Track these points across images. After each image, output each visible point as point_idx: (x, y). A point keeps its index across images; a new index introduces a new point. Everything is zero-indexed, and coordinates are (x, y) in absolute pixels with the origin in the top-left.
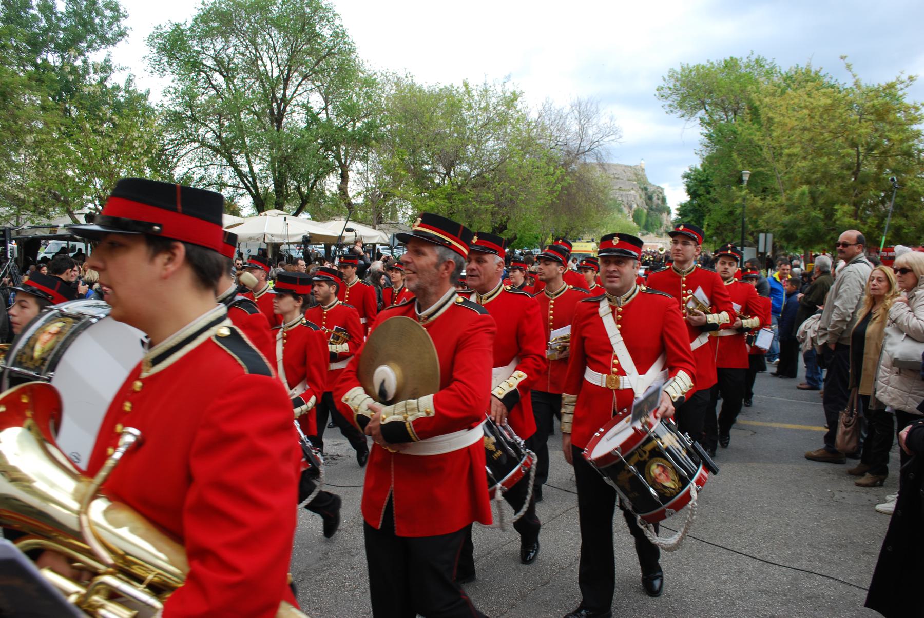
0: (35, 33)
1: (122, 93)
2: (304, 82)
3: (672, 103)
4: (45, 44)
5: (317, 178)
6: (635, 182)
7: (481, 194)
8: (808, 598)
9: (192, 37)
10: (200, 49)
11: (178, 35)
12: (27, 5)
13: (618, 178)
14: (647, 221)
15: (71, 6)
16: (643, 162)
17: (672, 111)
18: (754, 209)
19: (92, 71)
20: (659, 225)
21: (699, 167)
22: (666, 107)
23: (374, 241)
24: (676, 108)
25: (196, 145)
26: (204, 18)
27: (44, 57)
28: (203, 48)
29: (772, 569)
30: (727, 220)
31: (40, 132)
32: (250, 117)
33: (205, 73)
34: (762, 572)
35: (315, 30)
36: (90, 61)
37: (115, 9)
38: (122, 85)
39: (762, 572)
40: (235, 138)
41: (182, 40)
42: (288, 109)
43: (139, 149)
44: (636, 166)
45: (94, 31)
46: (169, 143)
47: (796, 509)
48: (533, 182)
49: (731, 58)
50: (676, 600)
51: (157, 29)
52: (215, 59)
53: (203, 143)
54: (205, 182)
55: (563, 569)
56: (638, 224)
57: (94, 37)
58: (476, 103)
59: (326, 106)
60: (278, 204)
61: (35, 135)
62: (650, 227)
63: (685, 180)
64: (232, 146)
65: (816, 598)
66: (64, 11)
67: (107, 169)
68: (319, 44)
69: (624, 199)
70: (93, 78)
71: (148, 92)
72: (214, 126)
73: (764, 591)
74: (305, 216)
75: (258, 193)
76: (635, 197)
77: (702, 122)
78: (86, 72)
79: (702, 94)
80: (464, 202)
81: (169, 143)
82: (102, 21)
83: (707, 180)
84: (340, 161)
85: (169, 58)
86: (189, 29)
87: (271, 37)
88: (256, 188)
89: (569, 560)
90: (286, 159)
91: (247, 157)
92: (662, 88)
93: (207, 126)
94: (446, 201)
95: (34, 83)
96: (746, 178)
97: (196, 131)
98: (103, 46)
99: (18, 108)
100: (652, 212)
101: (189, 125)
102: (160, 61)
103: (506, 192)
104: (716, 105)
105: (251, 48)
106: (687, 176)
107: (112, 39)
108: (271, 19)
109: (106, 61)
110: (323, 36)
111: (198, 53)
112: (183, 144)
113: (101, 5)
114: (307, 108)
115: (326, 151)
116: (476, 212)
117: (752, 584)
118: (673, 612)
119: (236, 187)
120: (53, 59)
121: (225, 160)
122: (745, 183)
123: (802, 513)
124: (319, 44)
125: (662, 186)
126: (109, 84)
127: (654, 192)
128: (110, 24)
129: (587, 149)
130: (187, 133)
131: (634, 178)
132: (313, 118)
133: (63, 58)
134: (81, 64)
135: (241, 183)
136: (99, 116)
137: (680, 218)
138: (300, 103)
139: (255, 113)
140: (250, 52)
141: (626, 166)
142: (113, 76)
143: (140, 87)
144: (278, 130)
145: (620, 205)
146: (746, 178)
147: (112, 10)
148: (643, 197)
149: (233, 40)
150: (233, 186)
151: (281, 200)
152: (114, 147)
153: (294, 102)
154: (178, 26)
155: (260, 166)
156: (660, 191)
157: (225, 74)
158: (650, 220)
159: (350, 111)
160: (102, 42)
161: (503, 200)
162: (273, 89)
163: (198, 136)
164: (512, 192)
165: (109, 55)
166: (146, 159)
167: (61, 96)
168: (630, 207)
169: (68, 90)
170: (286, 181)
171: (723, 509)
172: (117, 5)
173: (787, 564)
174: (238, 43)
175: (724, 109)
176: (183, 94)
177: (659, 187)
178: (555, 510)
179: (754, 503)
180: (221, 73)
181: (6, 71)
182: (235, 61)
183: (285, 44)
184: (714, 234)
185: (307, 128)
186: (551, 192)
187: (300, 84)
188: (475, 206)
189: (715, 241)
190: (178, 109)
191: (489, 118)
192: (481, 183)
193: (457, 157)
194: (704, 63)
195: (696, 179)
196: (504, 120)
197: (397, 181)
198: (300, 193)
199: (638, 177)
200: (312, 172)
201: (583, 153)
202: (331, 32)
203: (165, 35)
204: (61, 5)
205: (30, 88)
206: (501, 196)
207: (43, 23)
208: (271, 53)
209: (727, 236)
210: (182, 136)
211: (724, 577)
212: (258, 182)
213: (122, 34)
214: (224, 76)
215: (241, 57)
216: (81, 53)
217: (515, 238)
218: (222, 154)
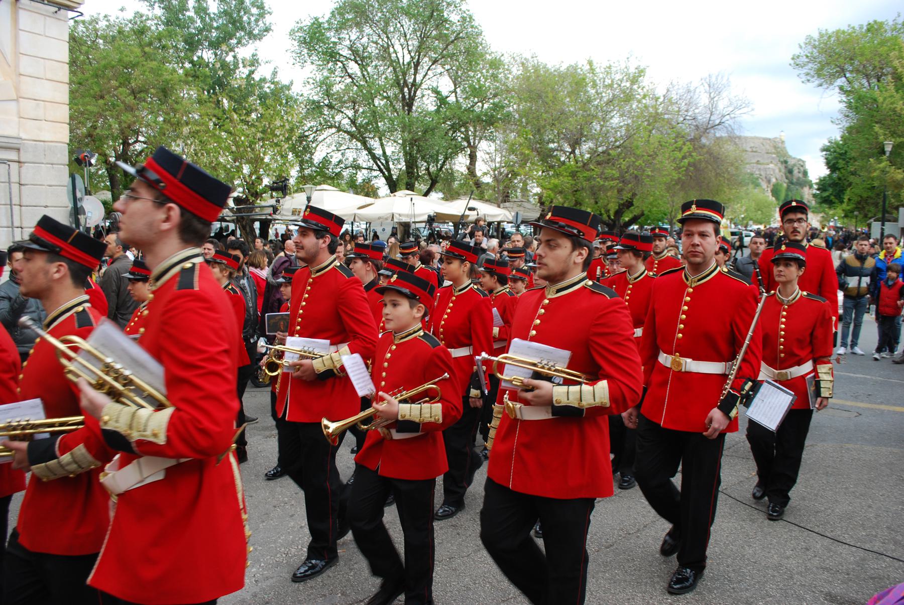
0: (190, 34)
1: (267, 85)
2: (433, 67)
3: (809, 71)
4: (199, 42)
5: (446, 159)
6: (774, 156)
7: (606, 171)
8: (871, 578)
9: (329, 29)
10: (337, 40)
11: (317, 28)
12: (183, 8)
15: (222, 6)
16: (782, 134)
17: (808, 81)
18: (894, 181)
19: (241, 65)
22: (802, 76)
23: (499, 219)
24: (813, 77)
25: (334, 130)
26: (340, 11)
27: (200, 54)
28: (339, 39)
29: (841, 549)
30: (870, 194)
31: (196, 123)
32: (382, 103)
33: (342, 62)
34: (830, 550)
35: (443, 16)
36: (240, 56)
37: (261, 7)
38: (269, 77)
39: (830, 550)
40: (367, 124)
41: (320, 32)
42: (419, 93)
43: (281, 137)
44: (776, 138)
45: (243, 29)
46: (309, 130)
47: (884, 492)
48: (659, 158)
49: (875, 22)
50: (734, 570)
51: (298, 23)
52: (350, 49)
53: (339, 129)
54: (342, 165)
55: (629, 534)
56: (777, 199)
57: (243, 34)
58: (600, 80)
59: (456, 88)
60: (409, 185)
61: (190, 126)
63: (824, 153)
64: (366, 129)
65: (880, 579)
66: (216, 12)
67: (253, 156)
68: (447, 29)
69: (762, 173)
70: (242, 72)
71: (292, 83)
72: (350, 113)
73: (826, 568)
74: (435, 196)
75: (391, 175)
76: (774, 170)
78: (236, 66)
79: (841, 60)
80: (588, 179)
81: (309, 130)
82: (249, 19)
83: (846, 152)
84: (469, 142)
85: (309, 49)
86: (327, 21)
87: (402, 26)
88: (389, 170)
89: (637, 527)
90: (416, 141)
91: (381, 140)
92: (798, 57)
93: (342, 112)
94: (570, 178)
95: (191, 79)
96: (888, 149)
97: (333, 118)
98: (251, 41)
99: (177, 103)
100: (792, 186)
101: (326, 113)
102: (300, 53)
104: (858, 71)
105: (384, 36)
107: (259, 34)
108: (402, 8)
109: (253, 55)
110: (451, 21)
111: (335, 43)
112: (321, 130)
113: (248, 4)
114: (436, 92)
115: (454, 132)
116: (601, 188)
117: (816, 561)
118: (728, 581)
119: (370, 169)
120: (207, 55)
121: (359, 144)
122: (888, 154)
123: (888, 497)
124: (447, 29)
125: (803, 159)
126: (257, 77)
127: (795, 165)
128: (257, 21)
129: (717, 122)
130: (324, 119)
131: (773, 151)
132: (442, 101)
133: (216, 55)
134: (232, 59)
135: (375, 165)
136: (245, 106)
137: (818, 192)
138: (430, 87)
139: (388, 98)
140: (383, 40)
142: (259, 69)
143: (283, 79)
144: (409, 114)
145: (757, 179)
146: (888, 149)
147: (258, 7)
148: (783, 170)
149: (367, 30)
150: (367, 169)
152: (259, 135)
153: (424, 86)
154: (317, 19)
155: (393, 149)
156: (801, 163)
157: (360, 62)
158: (790, 193)
159: (478, 93)
160: (250, 38)
161: (627, 176)
162: (404, 74)
163: (335, 122)
164: (639, 168)
165: (256, 50)
166: (287, 146)
167: (214, 89)
168: (769, 181)
169: (221, 85)
170: (416, 161)
171: (806, 487)
172: (262, 3)
173: (858, 545)
174: (371, 32)
175: (867, 77)
177: (800, 160)
180: (356, 62)
181: (166, 69)
182: (369, 49)
183: (415, 31)
184: (857, 208)
185: (438, 111)
186: (677, 168)
187: (429, 69)
188: (599, 183)
189: (856, 217)
190: (316, 98)
191: (614, 95)
192: (604, 159)
193: (582, 135)
194: (845, 28)
196: (628, 97)
197: (524, 160)
198: (429, 174)
199: (778, 150)
200: (441, 153)
201: (712, 127)
202: (458, 18)
203: (305, 28)
204: (213, 7)
205: (187, 83)
206: (626, 172)
207: (199, 23)
208: (402, 40)
209: (869, 211)
210: (321, 124)
211: (788, 553)
212: (391, 163)
213: (267, 30)
214: (359, 64)
215: (375, 45)
216: (232, 50)
218: (358, 140)
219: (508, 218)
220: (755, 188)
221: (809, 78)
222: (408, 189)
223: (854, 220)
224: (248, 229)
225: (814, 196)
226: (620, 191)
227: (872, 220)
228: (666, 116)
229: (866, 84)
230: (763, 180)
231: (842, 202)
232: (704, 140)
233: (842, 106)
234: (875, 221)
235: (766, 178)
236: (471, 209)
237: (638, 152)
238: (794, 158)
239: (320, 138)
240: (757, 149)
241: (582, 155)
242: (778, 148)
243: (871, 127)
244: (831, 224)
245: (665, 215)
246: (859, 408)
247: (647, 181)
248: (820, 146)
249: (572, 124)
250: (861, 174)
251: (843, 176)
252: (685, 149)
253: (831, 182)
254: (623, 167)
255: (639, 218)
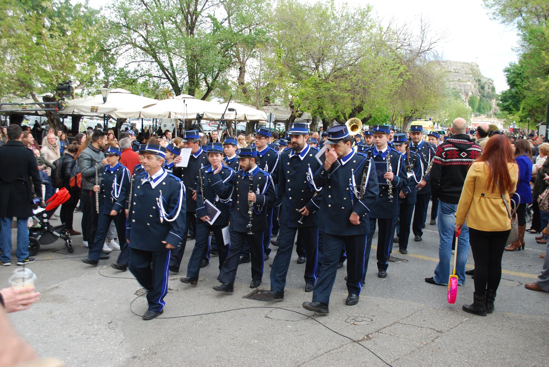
3: (495, 11)
6: (471, 76)
13: (458, 72)
14: (480, 105)
17: (495, 18)
20: (489, 109)
21: (517, 63)
24: (498, 15)
30: (538, 104)
38: (83, 3)
44: (472, 63)
48: (382, 75)
53: (135, 45)
56: (473, 107)
59: (229, 16)
62: (482, 110)
63: (506, 73)
69: (462, 88)
72: (144, 33)
77: (520, 26)
84: (239, 59)
88: (175, 78)
94: (313, 88)
100: (484, 98)
103: (360, 82)
106: (507, 70)
114: (214, 20)
127: (486, 83)
129: (426, 48)
131: (471, 72)
132: (217, 26)
137: (501, 102)
141: (464, 63)
145: (459, 92)
148: (477, 87)
151: (193, 87)
156: (490, 82)
158: (482, 103)
161: (357, 88)
164: (365, 83)
168: (467, 95)
175: (538, 16)
176: (119, 8)
177: (490, 79)
178: (319, 350)
179: (498, 353)
184: (529, 115)
190: (116, 20)
195: (514, 73)
206: (356, 85)
212: (176, 74)
217: (370, 117)
219: (264, 118)
220: (456, 99)
221: (495, 16)
222: (189, 94)
223: (527, 124)
224: (55, 122)
225: (498, 105)
226: (353, 99)
227: (540, 124)
228: (389, 43)
229: (537, 22)
230: (462, 94)
231: (518, 110)
232: (418, 63)
233: (519, 38)
234: (542, 124)
235: (465, 92)
236: (230, 110)
237: (366, 70)
238: (485, 78)
239: (120, 52)
240: (459, 71)
241: (324, 70)
242: (474, 70)
243: (540, 53)
244: (511, 127)
245: (387, 117)
246: (521, 277)
247: (373, 92)
248: (504, 68)
249: (315, 47)
250: (533, 89)
251: (520, 91)
252: (402, 69)
253: (511, 95)
254: (353, 81)
255: (368, 120)
